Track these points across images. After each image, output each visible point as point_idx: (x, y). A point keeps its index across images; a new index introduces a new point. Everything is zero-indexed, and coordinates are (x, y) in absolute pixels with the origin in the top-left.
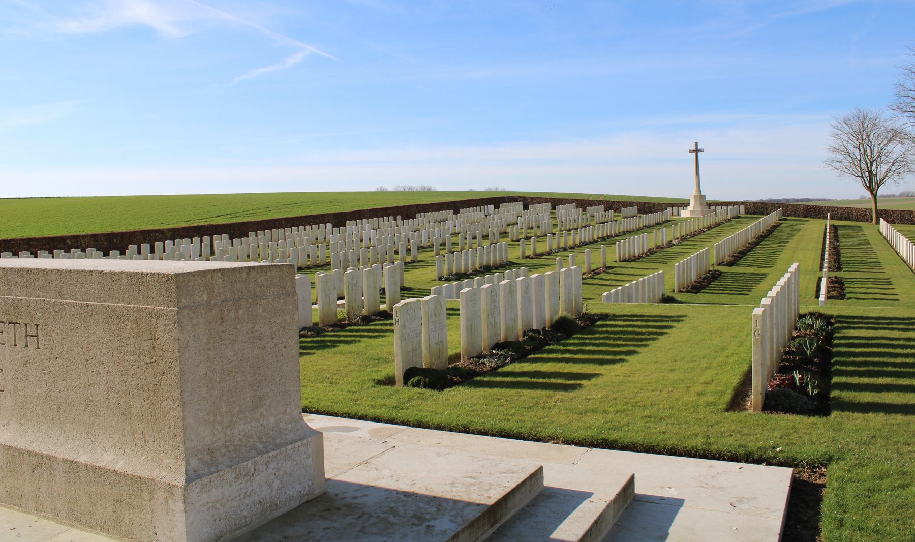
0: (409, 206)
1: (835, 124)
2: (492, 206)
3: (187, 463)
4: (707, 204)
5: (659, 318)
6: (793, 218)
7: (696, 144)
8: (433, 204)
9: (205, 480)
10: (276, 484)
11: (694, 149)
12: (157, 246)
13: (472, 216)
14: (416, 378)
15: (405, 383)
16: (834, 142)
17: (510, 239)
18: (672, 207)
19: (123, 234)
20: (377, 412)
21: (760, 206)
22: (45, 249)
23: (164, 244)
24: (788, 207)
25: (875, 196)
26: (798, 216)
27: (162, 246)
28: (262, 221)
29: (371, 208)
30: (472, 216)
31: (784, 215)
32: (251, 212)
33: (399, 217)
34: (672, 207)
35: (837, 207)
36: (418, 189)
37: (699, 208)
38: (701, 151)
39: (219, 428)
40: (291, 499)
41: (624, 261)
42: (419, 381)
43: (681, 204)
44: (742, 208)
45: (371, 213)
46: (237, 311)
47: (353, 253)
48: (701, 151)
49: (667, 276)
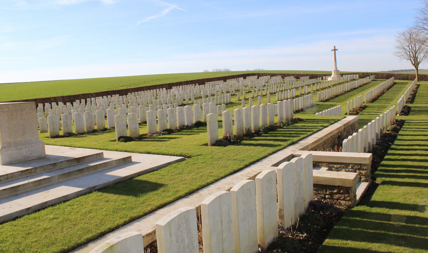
0: (203, 79)
1: (398, 35)
2: (242, 78)
3: (3, 145)
4: (340, 74)
5: (313, 127)
6: (381, 80)
7: (335, 47)
8: (215, 78)
9: (7, 149)
10: (29, 152)
11: (334, 49)
12: (88, 100)
13: (231, 83)
14: (121, 139)
15: (119, 141)
16: (398, 44)
17: (240, 93)
18: (325, 76)
19: (74, 95)
20: (96, 147)
21: (366, 74)
22: (48, 102)
23: (95, 98)
24: (379, 75)
25: (417, 69)
26: (383, 79)
27: (90, 100)
28: (134, 89)
29: (191, 80)
30: (231, 83)
31: (375, 78)
32: (137, 84)
33: (197, 84)
34: (325, 76)
35: (402, 74)
36: (223, 70)
37: (336, 76)
38: (336, 50)
39: (12, 139)
40: (34, 157)
41: (321, 101)
42: (122, 140)
43: (329, 74)
44: (357, 76)
45: (185, 83)
46: (17, 113)
47: (145, 100)
48: (336, 50)
49: (342, 108)
